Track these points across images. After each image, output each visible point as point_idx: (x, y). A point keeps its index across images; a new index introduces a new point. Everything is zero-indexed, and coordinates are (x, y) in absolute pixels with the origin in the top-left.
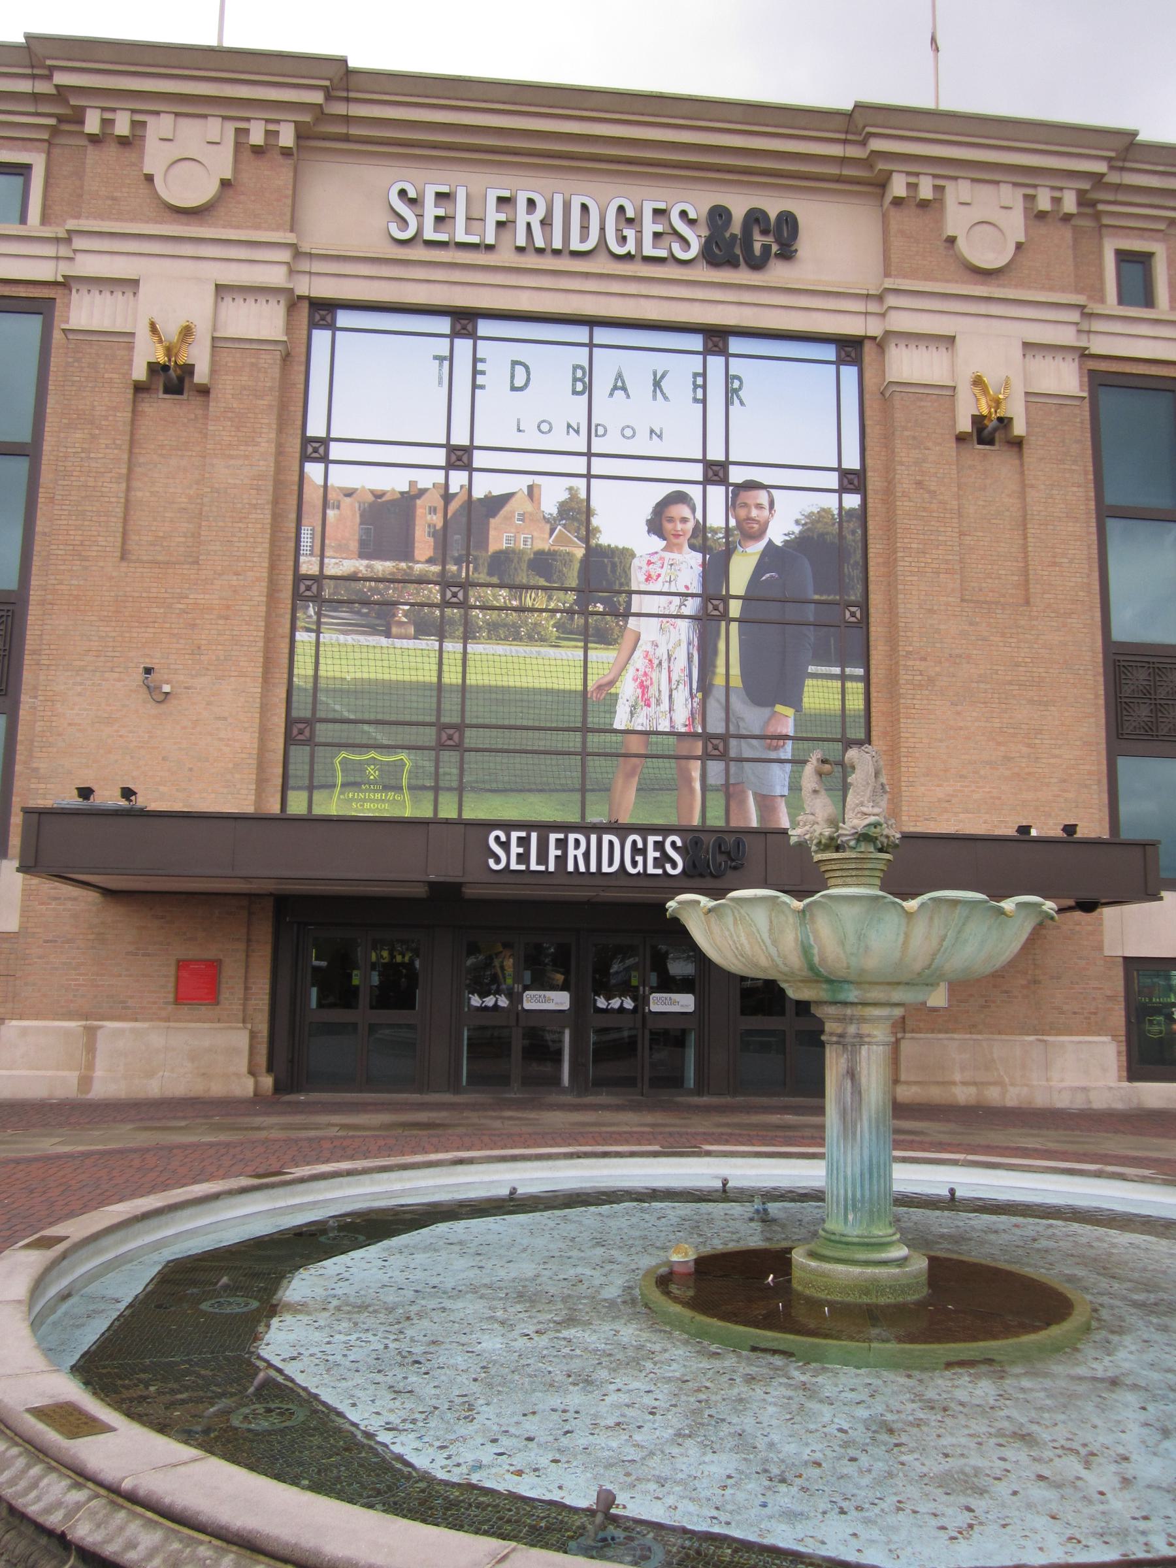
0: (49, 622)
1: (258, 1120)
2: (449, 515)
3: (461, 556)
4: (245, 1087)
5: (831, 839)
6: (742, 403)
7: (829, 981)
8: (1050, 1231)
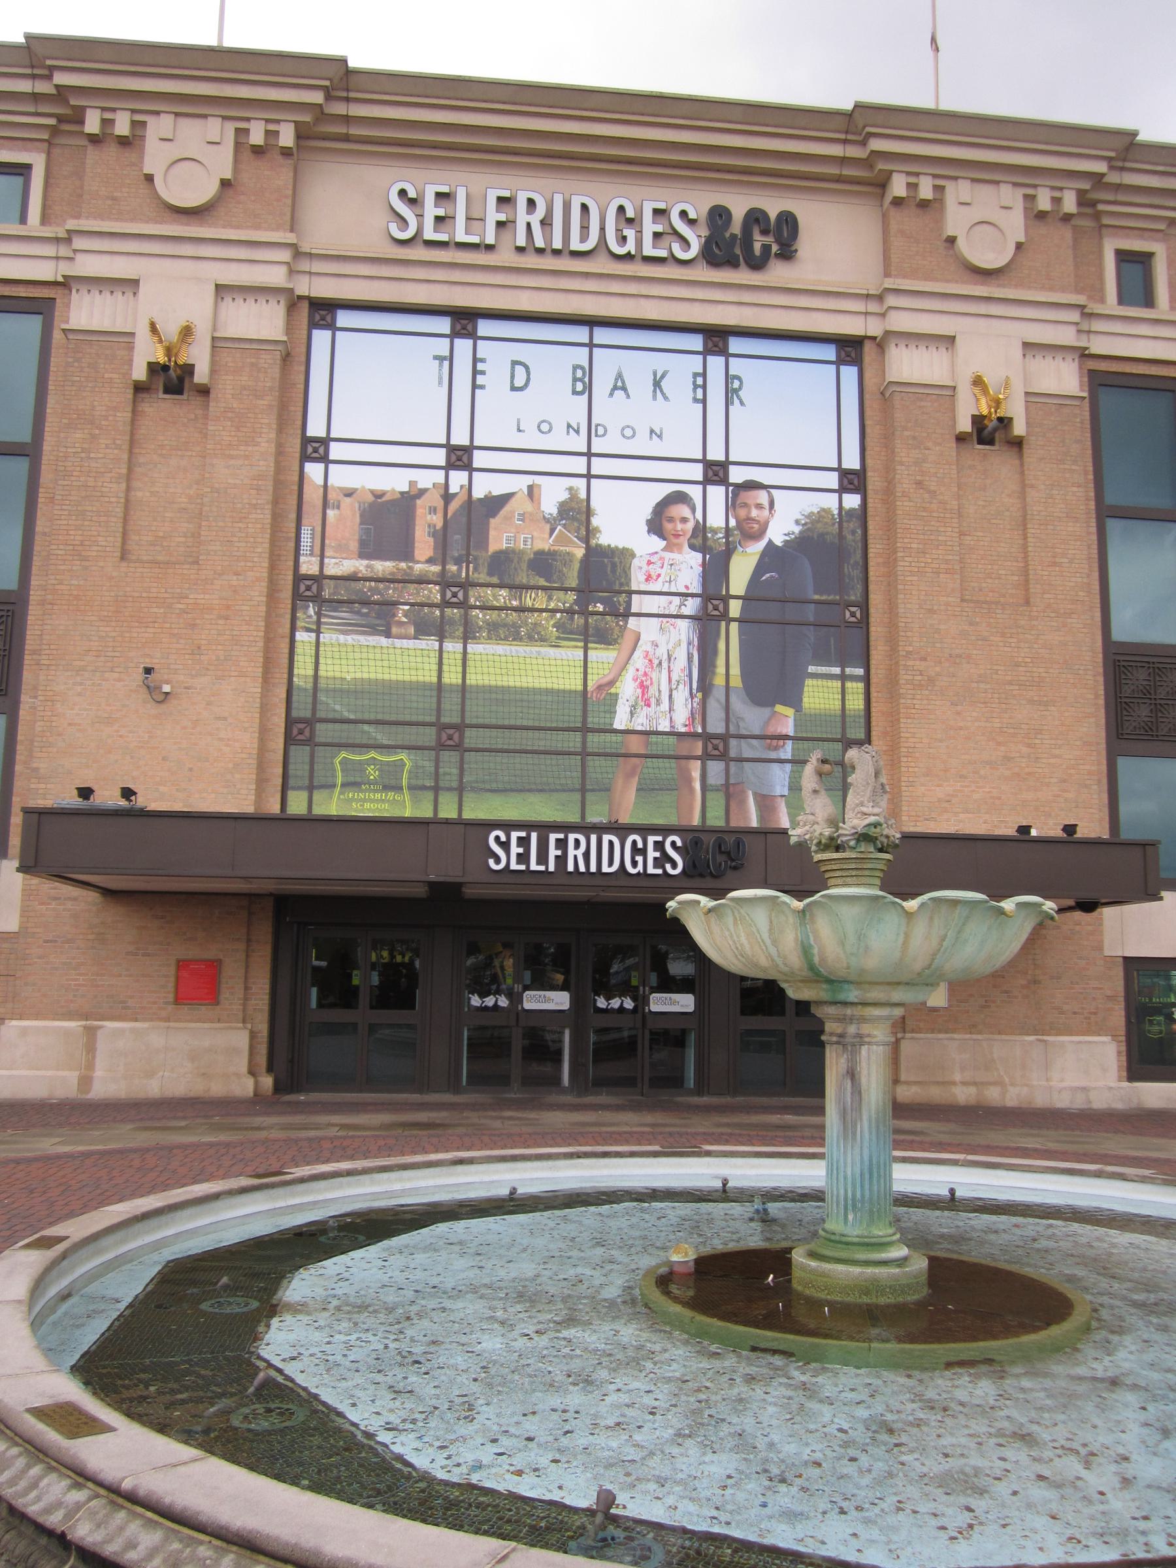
0: (49, 622)
1: (258, 1120)
2: (449, 515)
3: (461, 556)
4: (245, 1087)
5: (831, 839)
6: (742, 403)
7: (829, 981)
8: (1050, 1231)
